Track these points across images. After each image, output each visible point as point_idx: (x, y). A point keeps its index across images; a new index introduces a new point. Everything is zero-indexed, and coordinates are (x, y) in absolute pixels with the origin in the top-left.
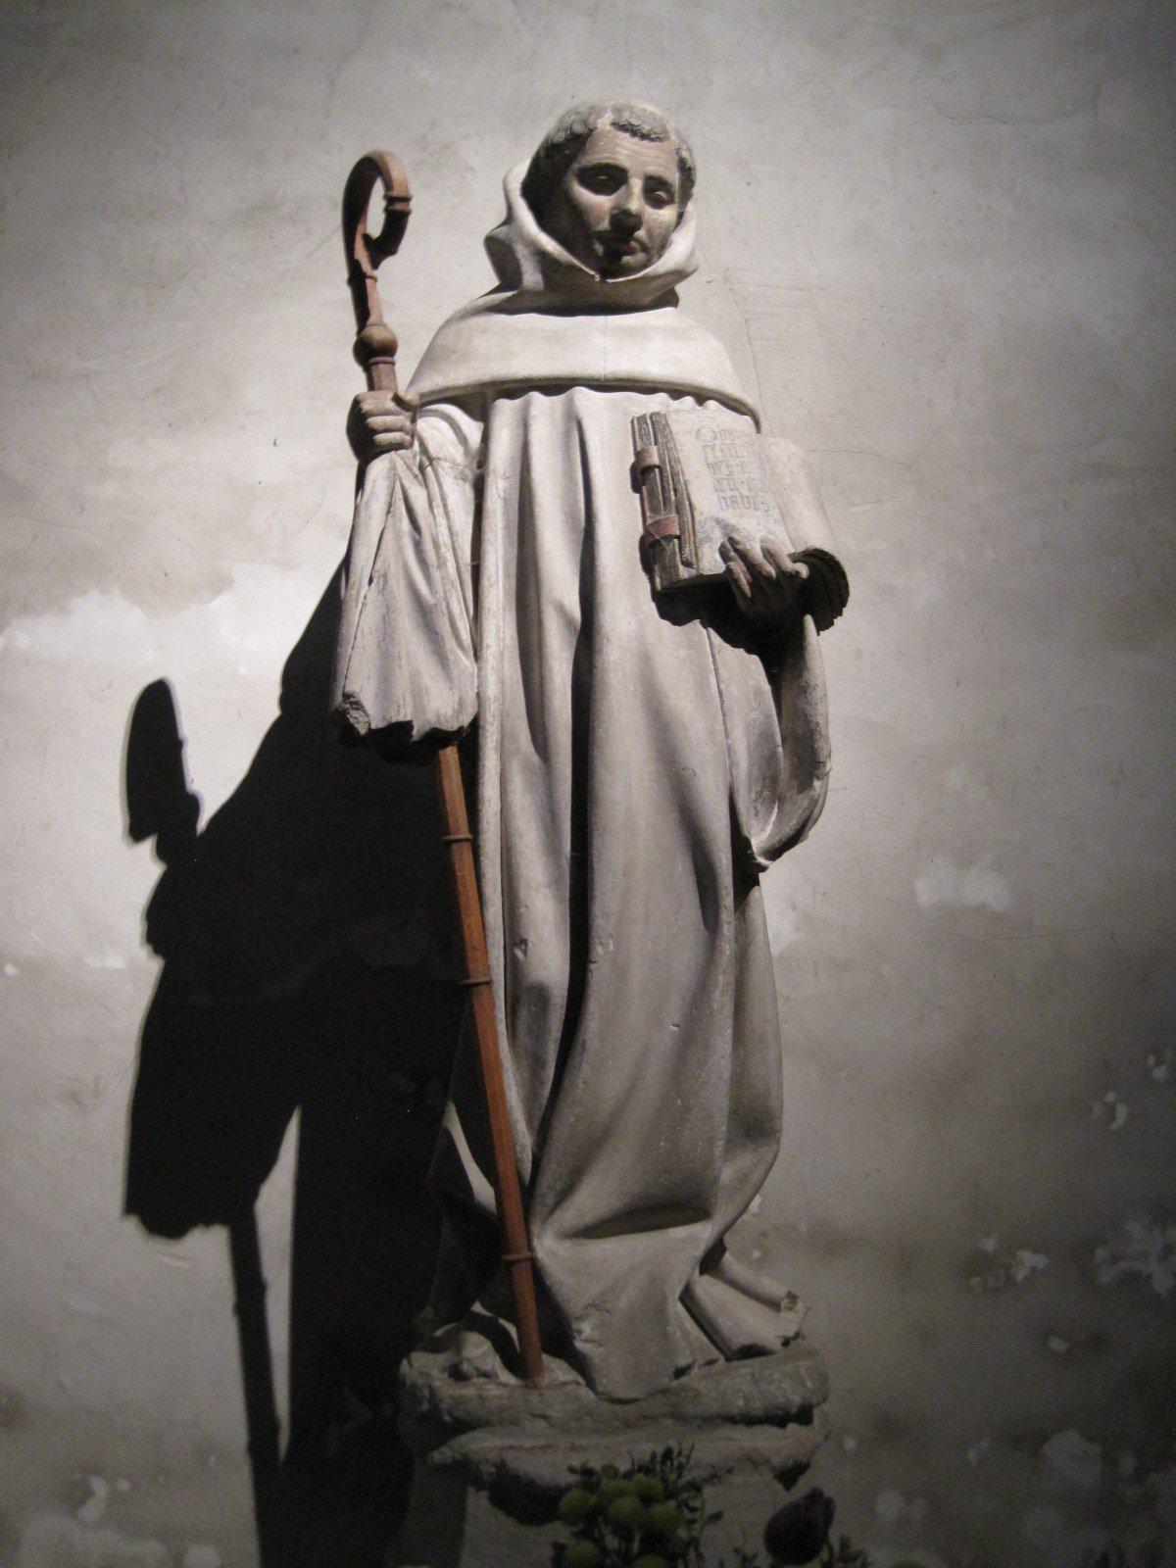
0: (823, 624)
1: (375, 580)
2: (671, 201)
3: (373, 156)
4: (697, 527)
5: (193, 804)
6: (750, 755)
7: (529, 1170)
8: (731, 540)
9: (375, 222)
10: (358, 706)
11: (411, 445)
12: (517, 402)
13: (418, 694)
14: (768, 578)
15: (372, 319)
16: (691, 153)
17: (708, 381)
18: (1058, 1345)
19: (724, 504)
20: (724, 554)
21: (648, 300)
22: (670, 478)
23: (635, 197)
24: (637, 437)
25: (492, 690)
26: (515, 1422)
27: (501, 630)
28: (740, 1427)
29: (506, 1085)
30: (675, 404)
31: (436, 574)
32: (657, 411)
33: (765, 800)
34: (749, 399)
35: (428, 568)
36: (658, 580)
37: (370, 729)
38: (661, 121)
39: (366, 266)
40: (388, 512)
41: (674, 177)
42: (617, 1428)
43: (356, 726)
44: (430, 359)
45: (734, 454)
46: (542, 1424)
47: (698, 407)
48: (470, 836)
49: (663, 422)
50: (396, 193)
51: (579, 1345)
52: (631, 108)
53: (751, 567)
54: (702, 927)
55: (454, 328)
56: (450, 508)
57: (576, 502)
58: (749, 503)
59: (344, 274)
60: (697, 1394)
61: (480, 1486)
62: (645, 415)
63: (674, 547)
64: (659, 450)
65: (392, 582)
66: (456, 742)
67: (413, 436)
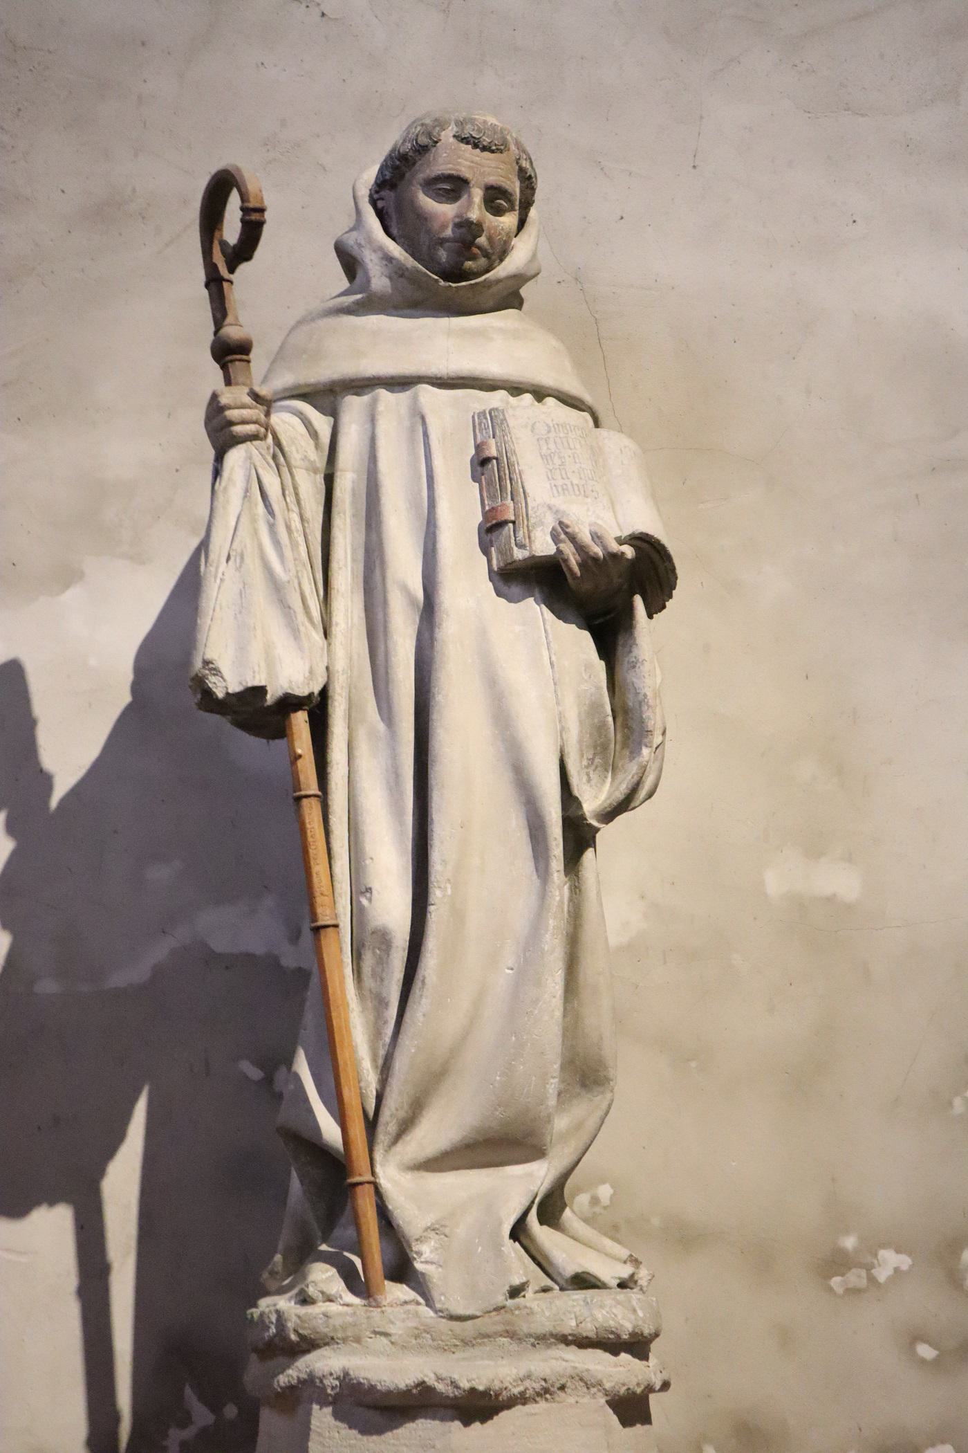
0: (653, 609)
1: (232, 558)
2: (512, 209)
3: (230, 169)
4: (530, 512)
5: (45, 781)
6: (581, 722)
7: (374, 1105)
8: (561, 523)
9: (231, 230)
10: (216, 672)
11: (266, 436)
12: (366, 399)
13: (271, 663)
14: (595, 559)
15: (229, 319)
16: (531, 163)
17: (547, 379)
18: (926, 1352)
19: (555, 492)
20: (555, 538)
21: (491, 303)
22: (506, 467)
23: (476, 207)
24: (477, 431)
25: (340, 665)
26: (358, 1340)
27: (350, 610)
28: (573, 1348)
29: (351, 1025)
30: (513, 400)
31: (288, 553)
32: (495, 407)
33: (596, 767)
34: (588, 398)
35: (281, 548)
36: (495, 562)
37: (228, 694)
38: (502, 133)
39: (223, 271)
40: (245, 497)
41: (515, 187)
42: (456, 1346)
43: (214, 690)
44: (280, 357)
45: (566, 444)
46: (384, 1340)
47: (536, 403)
48: (320, 793)
49: (501, 417)
50: (252, 204)
51: (418, 1266)
52: (472, 121)
53: (580, 548)
54: (535, 877)
55: (305, 328)
56: (301, 496)
57: (420, 491)
58: (579, 490)
59: (201, 275)
60: (531, 1313)
61: (323, 1404)
62: (484, 411)
63: (509, 531)
64: (496, 443)
65: (248, 560)
66: (306, 708)
67: (267, 429)
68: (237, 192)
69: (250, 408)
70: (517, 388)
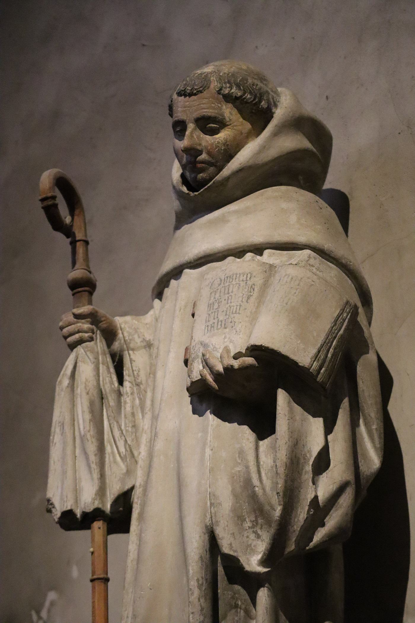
68: (177, 160)
69: (74, 324)
70: (241, 252)
